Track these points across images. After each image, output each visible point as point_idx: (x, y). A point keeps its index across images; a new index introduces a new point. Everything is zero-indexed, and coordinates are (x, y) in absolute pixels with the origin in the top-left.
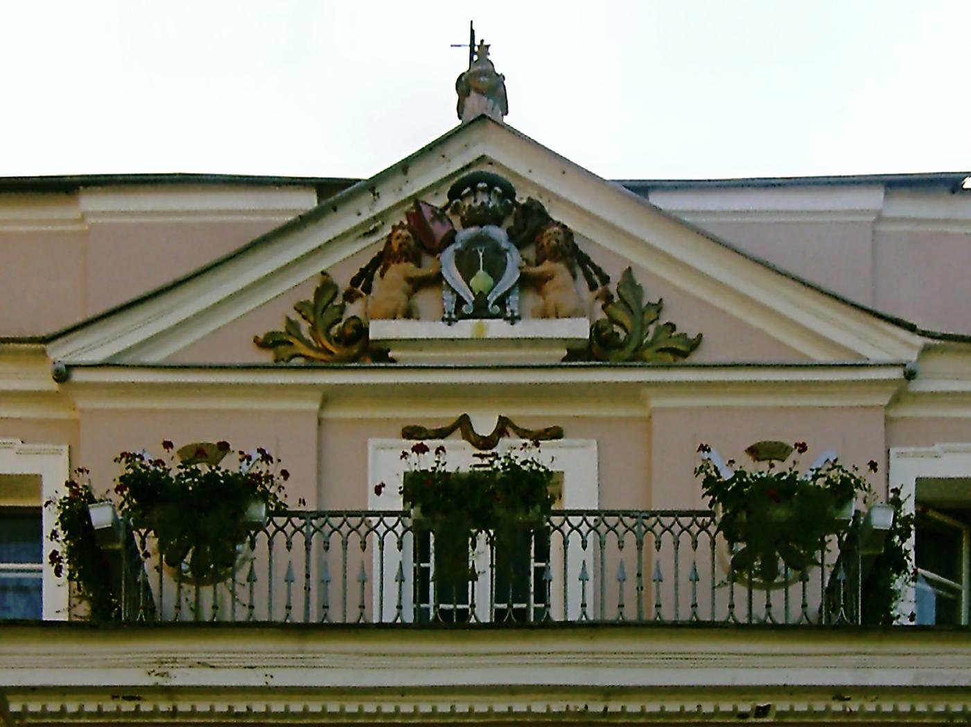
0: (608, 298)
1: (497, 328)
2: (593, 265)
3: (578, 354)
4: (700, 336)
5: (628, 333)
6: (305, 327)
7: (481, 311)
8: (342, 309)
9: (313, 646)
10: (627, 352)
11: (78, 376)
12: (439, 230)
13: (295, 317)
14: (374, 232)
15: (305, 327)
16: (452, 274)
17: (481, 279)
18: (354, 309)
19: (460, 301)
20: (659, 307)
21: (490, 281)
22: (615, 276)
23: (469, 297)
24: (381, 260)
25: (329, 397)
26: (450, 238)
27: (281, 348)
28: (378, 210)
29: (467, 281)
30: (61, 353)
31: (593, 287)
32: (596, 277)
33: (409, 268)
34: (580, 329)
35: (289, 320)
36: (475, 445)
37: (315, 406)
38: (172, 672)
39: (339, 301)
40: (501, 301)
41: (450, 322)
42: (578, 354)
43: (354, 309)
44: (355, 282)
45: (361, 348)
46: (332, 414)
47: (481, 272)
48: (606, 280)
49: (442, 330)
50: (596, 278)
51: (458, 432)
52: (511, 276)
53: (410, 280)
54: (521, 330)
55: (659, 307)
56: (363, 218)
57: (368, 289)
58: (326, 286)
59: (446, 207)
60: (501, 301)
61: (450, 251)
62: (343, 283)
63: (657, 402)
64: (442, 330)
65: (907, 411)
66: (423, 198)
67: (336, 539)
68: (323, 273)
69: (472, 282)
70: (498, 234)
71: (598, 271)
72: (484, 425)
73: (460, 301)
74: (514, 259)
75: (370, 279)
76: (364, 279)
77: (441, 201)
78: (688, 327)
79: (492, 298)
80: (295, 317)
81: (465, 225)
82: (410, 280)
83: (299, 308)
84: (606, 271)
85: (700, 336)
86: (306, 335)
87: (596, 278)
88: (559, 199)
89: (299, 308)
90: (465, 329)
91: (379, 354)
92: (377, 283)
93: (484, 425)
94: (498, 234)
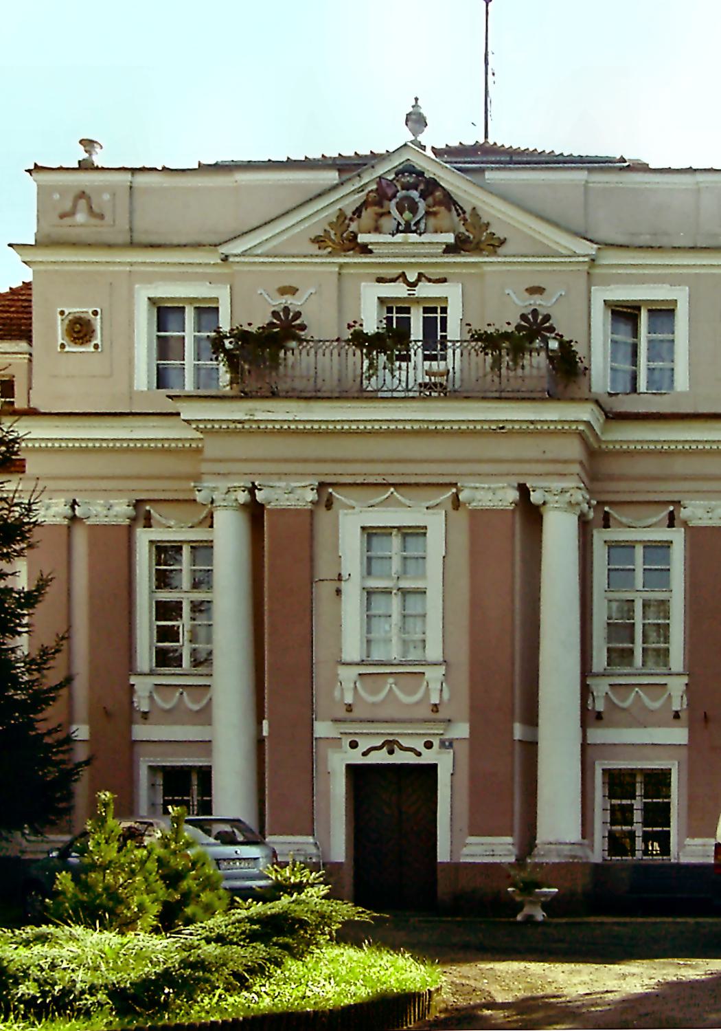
0: (465, 220)
1: (413, 237)
2: (459, 206)
3: (450, 249)
4: (505, 239)
5: (474, 240)
6: (332, 232)
7: (408, 230)
8: (348, 226)
9: (313, 404)
10: (473, 245)
11: (231, 259)
12: (390, 192)
13: (328, 228)
14: (363, 191)
15: (332, 232)
16: (395, 212)
17: (407, 215)
18: (353, 227)
19: (399, 224)
20: (488, 225)
21: (411, 215)
22: (468, 209)
23: (403, 223)
24: (365, 204)
25: (341, 266)
26: (394, 196)
27: (322, 244)
28: (362, 183)
29: (402, 215)
30: (224, 250)
31: (459, 215)
32: (461, 211)
33: (376, 209)
34: (450, 238)
35: (325, 230)
36: (408, 285)
37: (337, 269)
38: (256, 414)
39: (347, 221)
40: (417, 223)
41: (393, 235)
42: (450, 249)
43: (353, 227)
44: (354, 213)
45: (353, 245)
46: (344, 271)
47: (407, 212)
48: (464, 212)
49: (389, 238)
50: (460, 211)
51: (401, 279)
52: (421, 212)
53: (377, 214)
54: (425, 238)
55: (488, 225)
56: (355, 187)
57: (359, 217)
58: (341, 214)
59: (394, 179)
60: (417, 223)
61: (394, 202)
62: (349, 214)
63: (487, 268)
64: (389, 238)
65: (597, 271)
66: (384, 176)
67: (327, 352)
68: (340, 209)
69: (404, 215)
70: (415, 194)
71: (461, 208)
72: (412, 278)
73: (399, 224)
74: (422, 205)
75: (361, 212)
76: (358, 212)
77: (391, 177)
78: (500, 234)
79: (413, 223)
80: (328, 228)
81: (403, 189)
82: (377, 214)
83: (330, 224)
84: (465, 208)
85: (505, 239)
86: (333, 237)
87: (460, 211)
88: (443, 179)
89: (330, 224)
90: (400, 237)
91: (365, 249)
92: (364, 213)
93: (412, 278)
94: (415, 194)
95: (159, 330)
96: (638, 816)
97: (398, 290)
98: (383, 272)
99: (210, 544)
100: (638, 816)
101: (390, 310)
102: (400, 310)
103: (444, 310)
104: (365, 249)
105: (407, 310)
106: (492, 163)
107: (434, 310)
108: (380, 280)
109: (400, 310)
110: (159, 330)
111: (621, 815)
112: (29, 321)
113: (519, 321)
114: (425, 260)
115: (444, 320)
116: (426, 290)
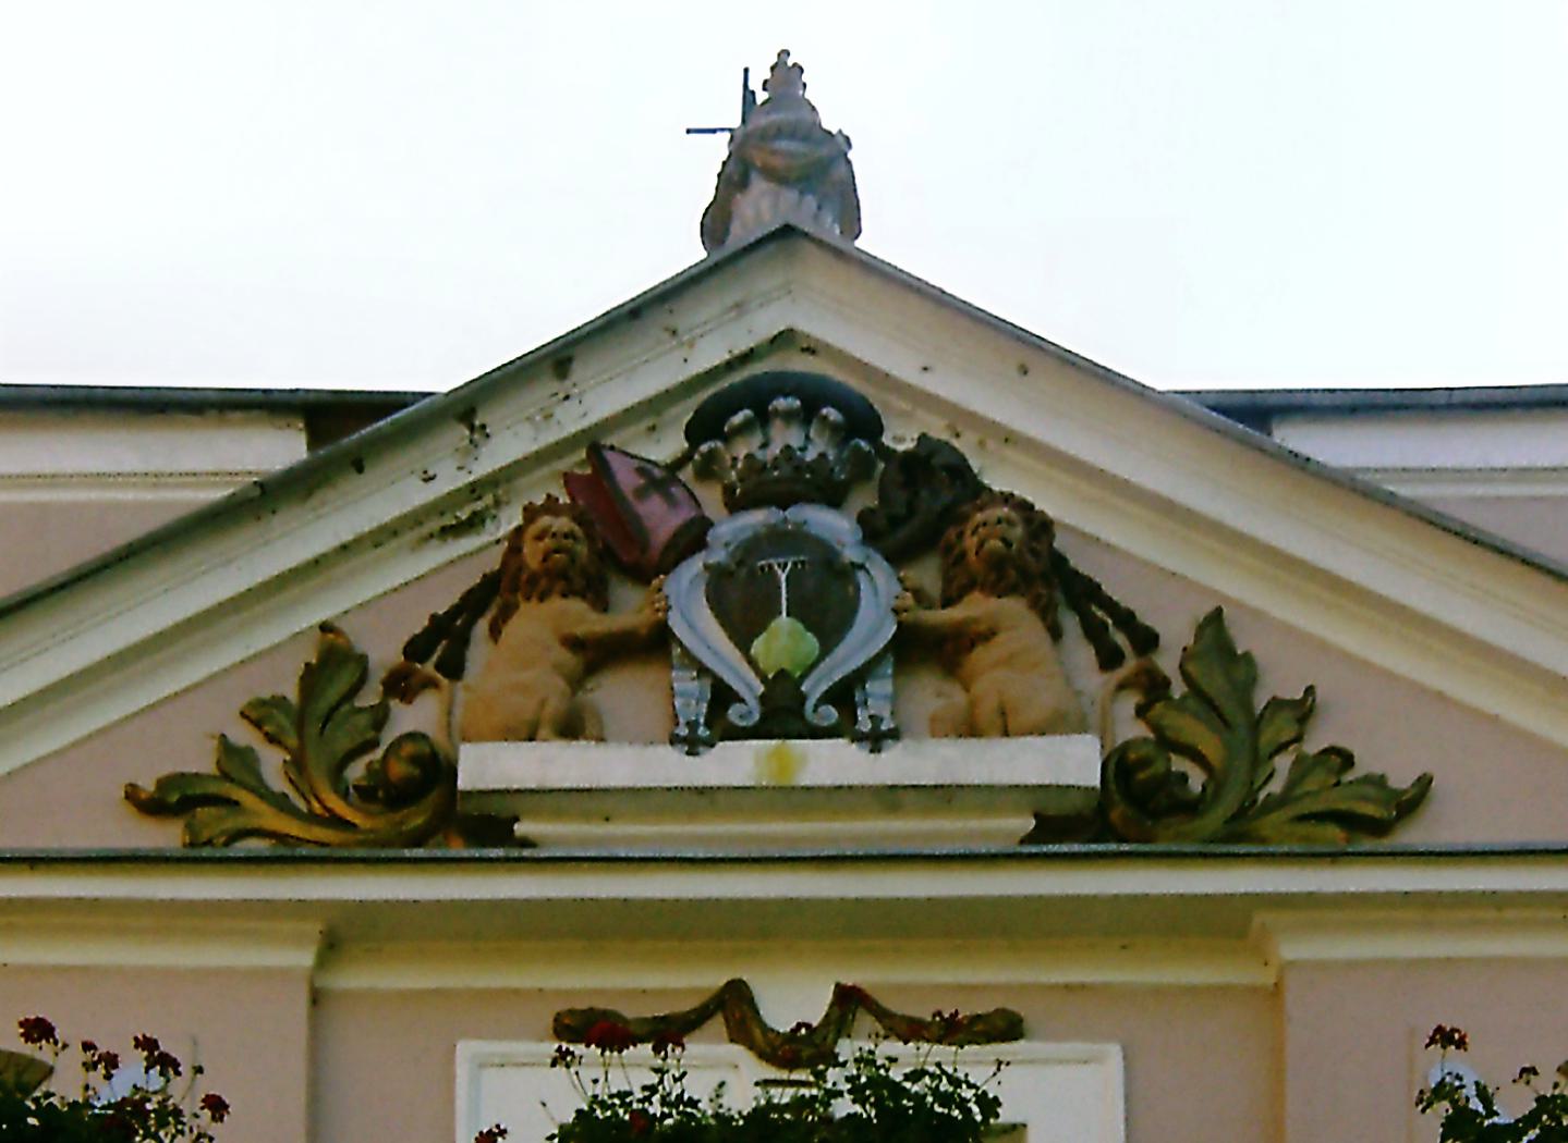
3: (1063, 826)
61: (694, 566)
70: (836, 526)
90: (736, 763)
104: (489, 828)
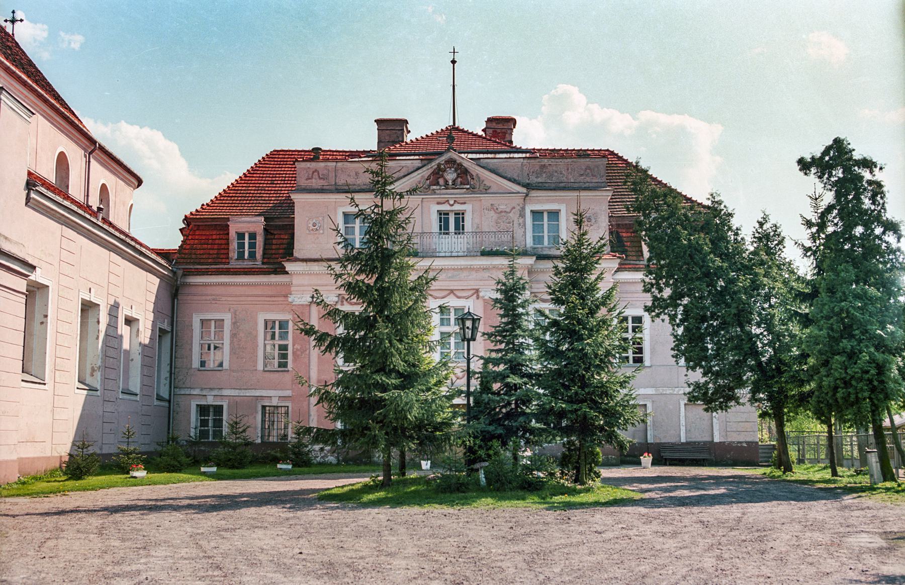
78: (488, 184)
95: (633, 318)
96: (211, 424)
97: (445, 207)
98: (439, 200)
99: (265, 260)
100: (211, 424)
101: (440, 214)
102: (445, 214)
103: (463, 214)
105: (448, 214)
106: (141, 253)
107: (459, 214)
108: (438, 203)
109: (445, 214)
110: (633, 318)
111: (204, 423)
112: (265, 260)
113: (809, 231)
114: (117, 234)
115: (463, 218)
116: (457, 207)
